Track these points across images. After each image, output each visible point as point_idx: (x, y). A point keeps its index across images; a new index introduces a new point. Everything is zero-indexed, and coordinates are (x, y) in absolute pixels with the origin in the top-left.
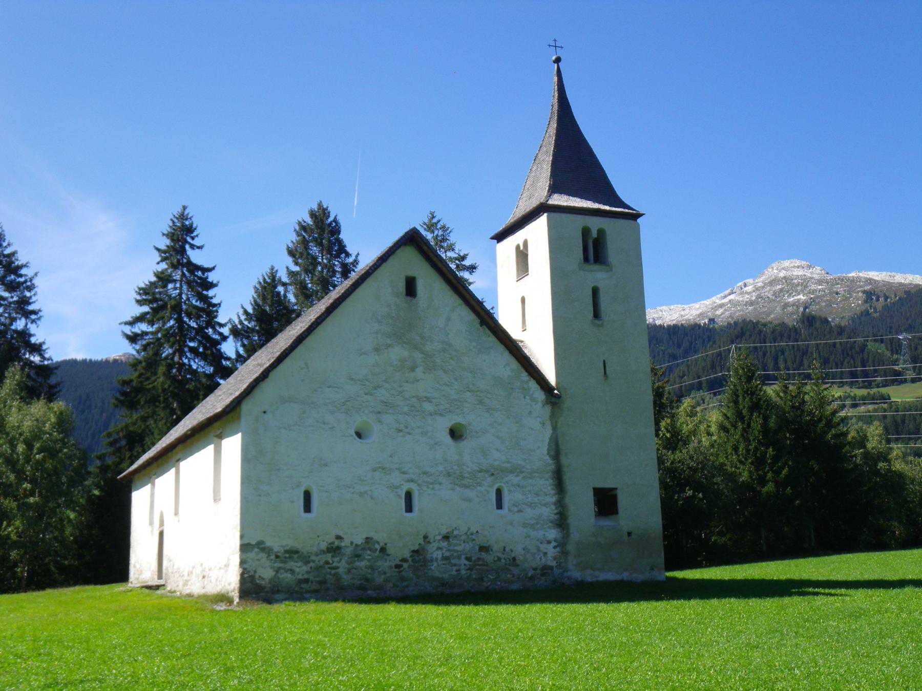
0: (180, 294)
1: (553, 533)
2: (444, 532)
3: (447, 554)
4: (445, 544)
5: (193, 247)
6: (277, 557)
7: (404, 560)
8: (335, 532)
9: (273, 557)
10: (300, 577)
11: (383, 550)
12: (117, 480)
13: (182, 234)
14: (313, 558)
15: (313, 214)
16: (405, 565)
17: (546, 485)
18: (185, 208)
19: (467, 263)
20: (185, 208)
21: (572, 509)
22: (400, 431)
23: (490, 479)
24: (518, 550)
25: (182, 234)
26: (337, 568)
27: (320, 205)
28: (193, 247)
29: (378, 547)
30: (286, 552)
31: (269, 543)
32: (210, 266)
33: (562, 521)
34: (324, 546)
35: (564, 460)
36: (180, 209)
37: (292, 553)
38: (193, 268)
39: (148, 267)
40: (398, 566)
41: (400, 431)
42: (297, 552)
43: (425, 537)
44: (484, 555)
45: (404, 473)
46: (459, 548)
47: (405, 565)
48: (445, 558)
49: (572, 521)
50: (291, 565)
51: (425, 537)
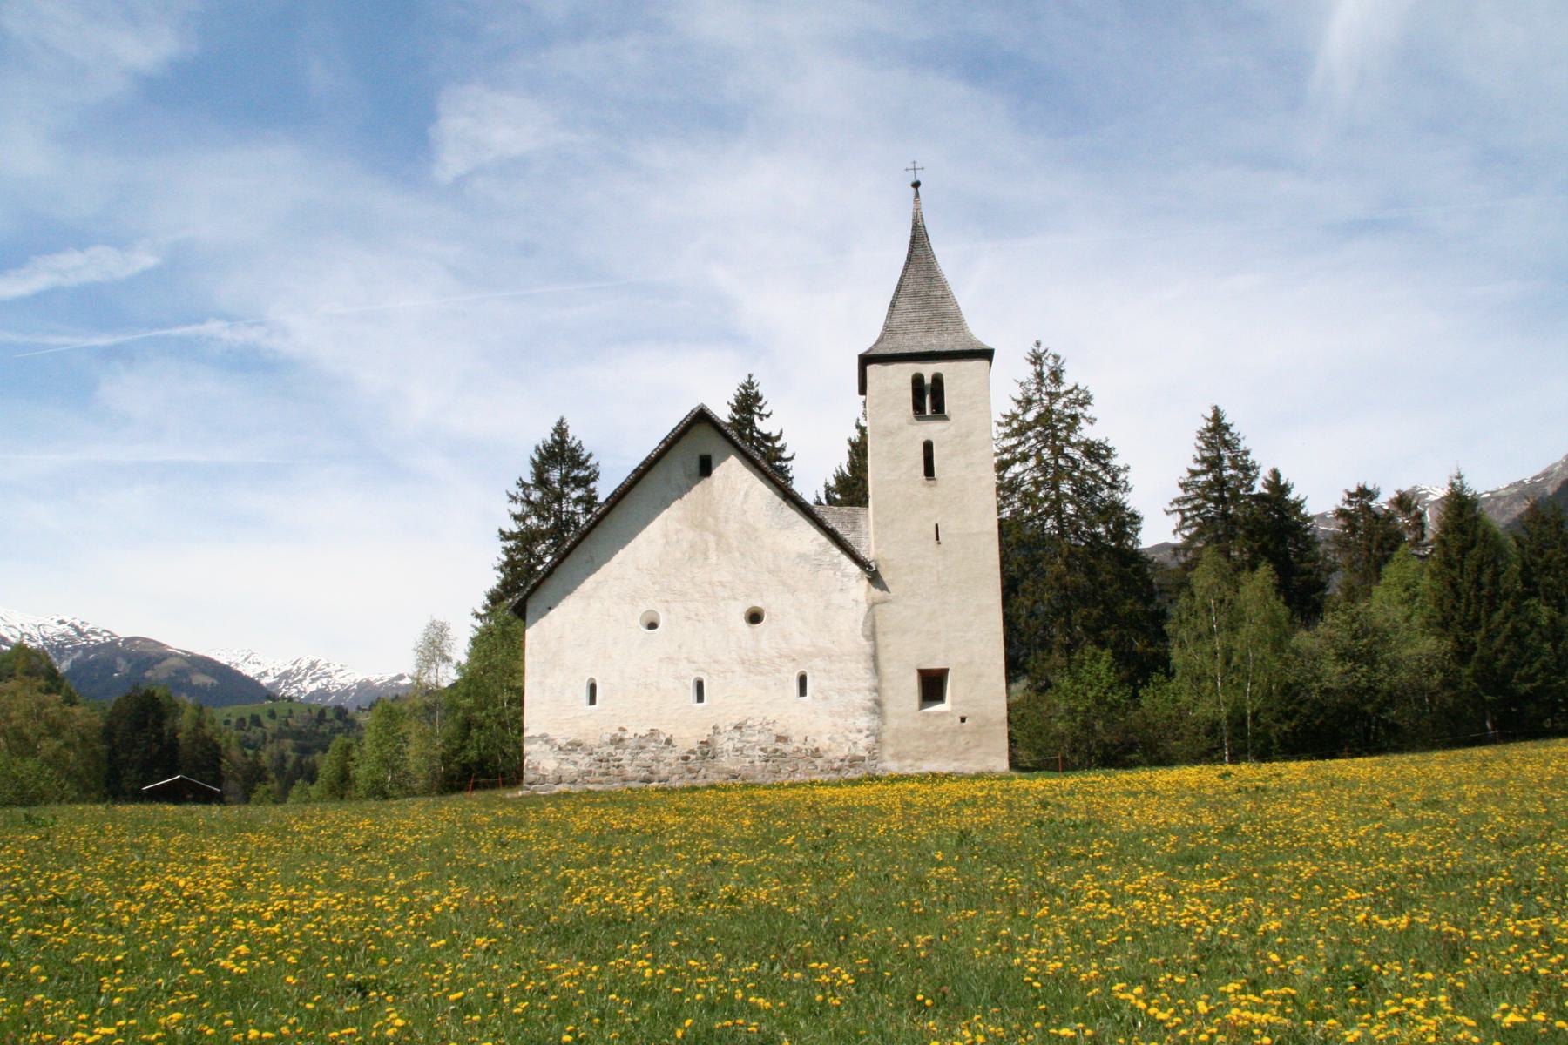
1: (864, 721)
21: (889, 694)
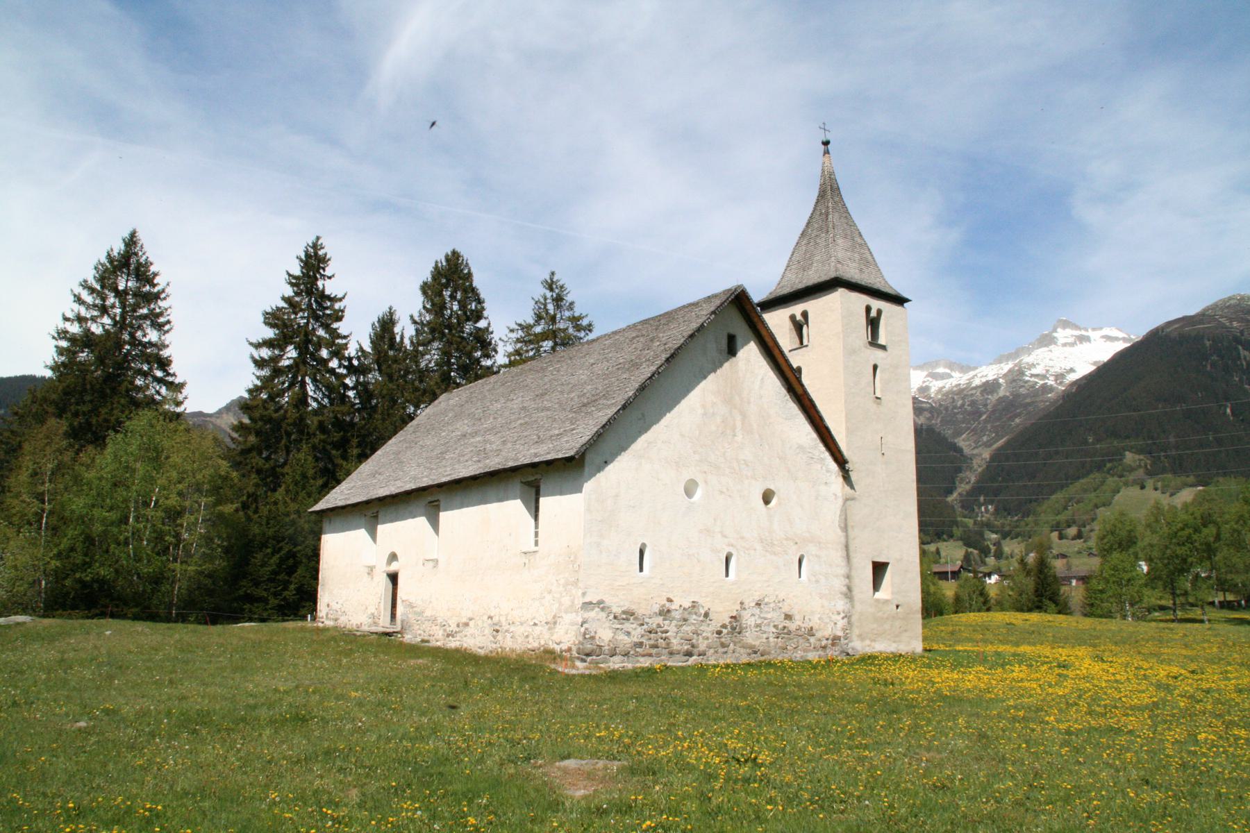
0: (307, 324)
1: (841, 604)
2: (757, 598)
3: (759, 622)
4: (757, 611)
5: (323, 276)
6: (615, 617)
7: (724, 626)
8: (665, 595)
9: (611, 617)
10: (636, 640)
11: (706, 615)
12: (1148, 573)
13: (314, 262)
14: (647, 620)
15: (447, 260)
16: (725, 631)
17: (837, 556)
18: (318, 238)
19: (585, 322)
20: (318, 238)
22: (722, 492)
23: (795, 547)
24: (815, 622)
25: (314, 262)
26: (667, 632)
27: (454, 252)
28: (323, 276)
29: (702, 611)
30: (624, 612)
31: (609, 601)
32: (339, 296)
33: (849, 593)
34: (656, 609)
35: (851, 533)
36: (313, 238)
37: (629, 614)
38: (323, 296)
39: (276, 292)
40: (719, 633)
41: (722, 492)
42: (633, 614)
43: (742, 603)
44: (787, 623)
45: (725, 536)
46: (769, 616)
47: (725, 631)
48: (758, 626)
49: (856, 592)
50: (628, 626)
51: (742, 603)
